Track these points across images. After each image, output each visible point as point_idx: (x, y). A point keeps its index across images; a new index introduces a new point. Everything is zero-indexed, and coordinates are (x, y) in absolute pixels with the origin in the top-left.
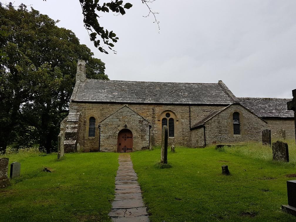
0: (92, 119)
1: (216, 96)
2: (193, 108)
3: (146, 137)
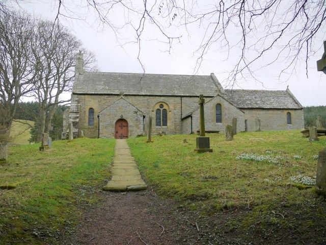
0: (91, 110)
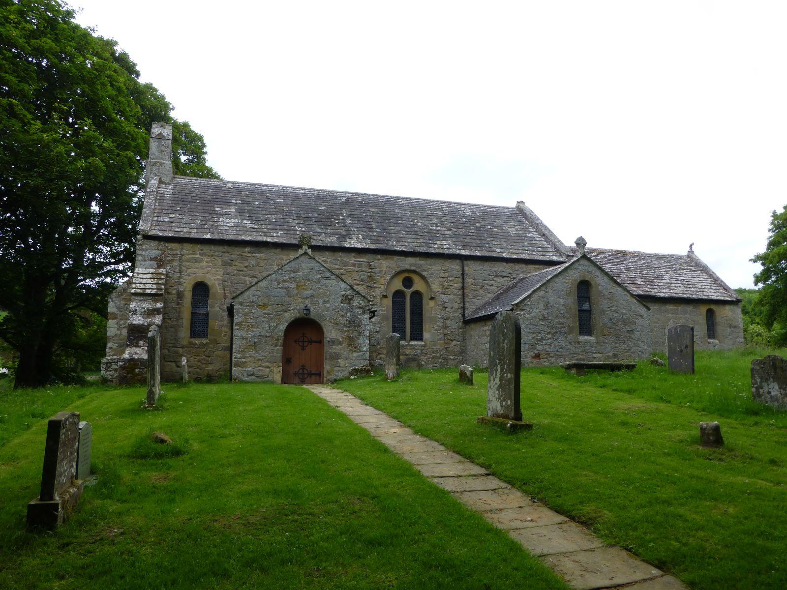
0: (201, 290)
1: (518, 238)
2: (471, 268)
3: (361, 340)
